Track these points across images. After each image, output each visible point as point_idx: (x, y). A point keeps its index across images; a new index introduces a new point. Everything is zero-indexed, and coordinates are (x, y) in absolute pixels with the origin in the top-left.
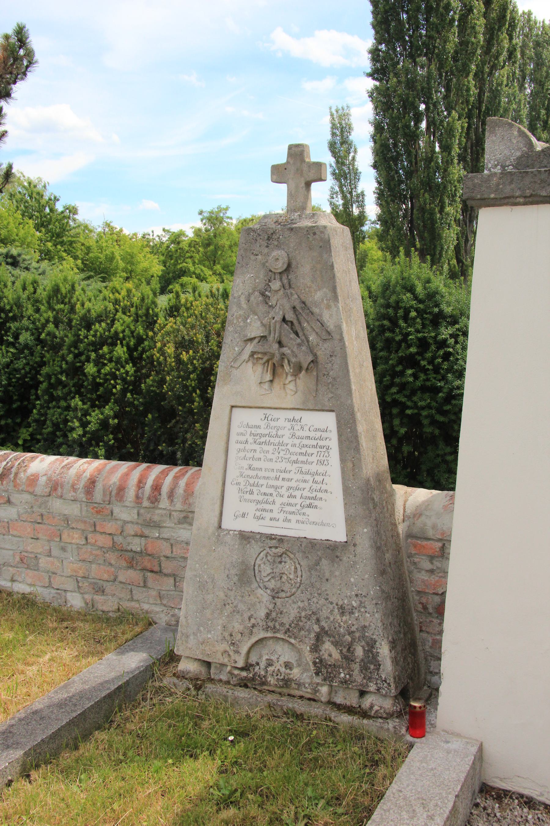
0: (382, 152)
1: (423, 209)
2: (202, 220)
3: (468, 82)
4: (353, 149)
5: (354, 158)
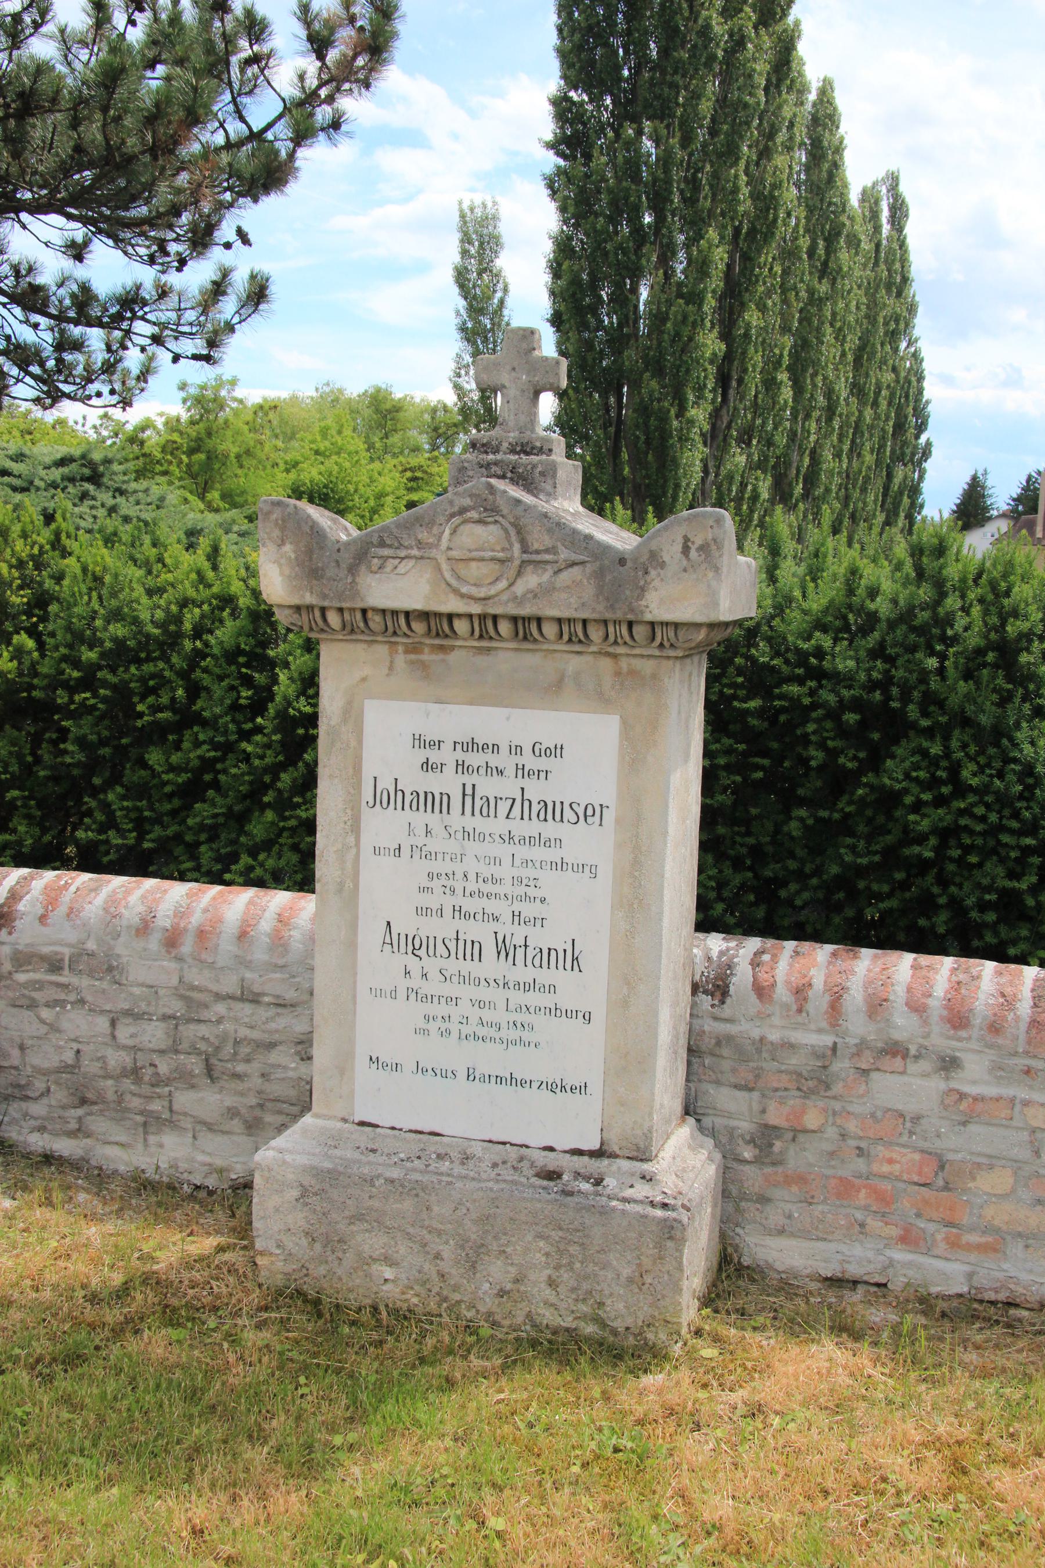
0: (574, 295)
1: (646, 408)
2: (184, 401)
3: (736, 176)
4: (500, 286)
5: (502, 302)
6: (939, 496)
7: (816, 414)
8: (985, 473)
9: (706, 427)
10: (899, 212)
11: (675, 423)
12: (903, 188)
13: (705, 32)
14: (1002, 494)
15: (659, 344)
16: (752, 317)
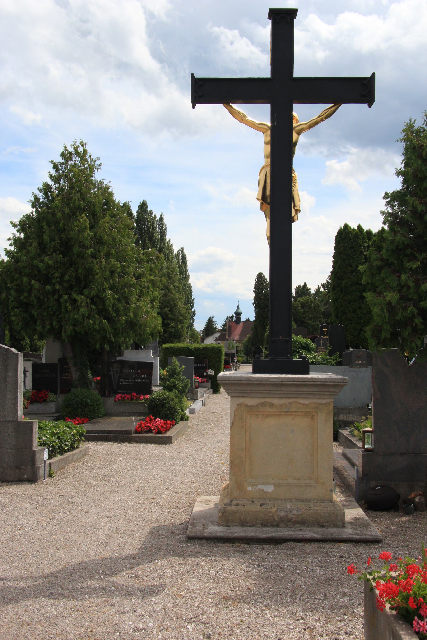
6: (199, 326)
8: (213, 317)
12: (185, 251)
14: (219, 324)
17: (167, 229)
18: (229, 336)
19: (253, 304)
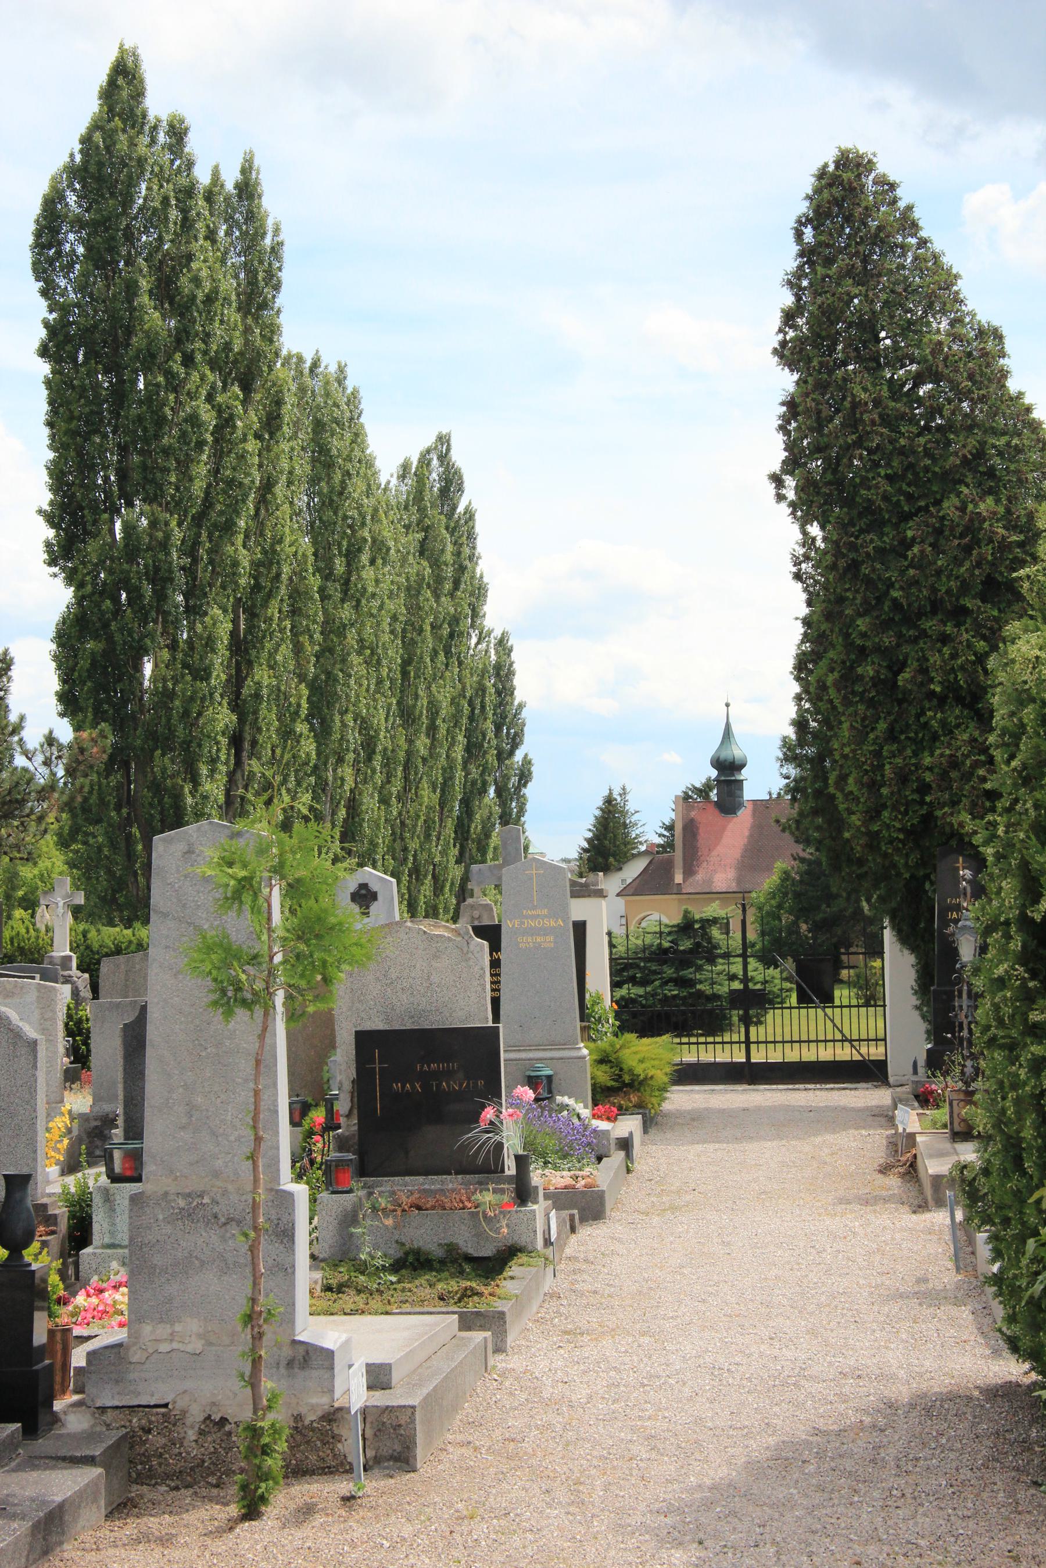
7: (350, 756)
8: (624, 792)
9: (221, 798)
10: (452, 483)
11: (189, 800)
12: (457, 456)
13: (193, 419)
14: (650, 820)
15: (169, 720)
16: (262, 675)
17: (287, 253)
18: (689, 871)
19: (777, 480)
